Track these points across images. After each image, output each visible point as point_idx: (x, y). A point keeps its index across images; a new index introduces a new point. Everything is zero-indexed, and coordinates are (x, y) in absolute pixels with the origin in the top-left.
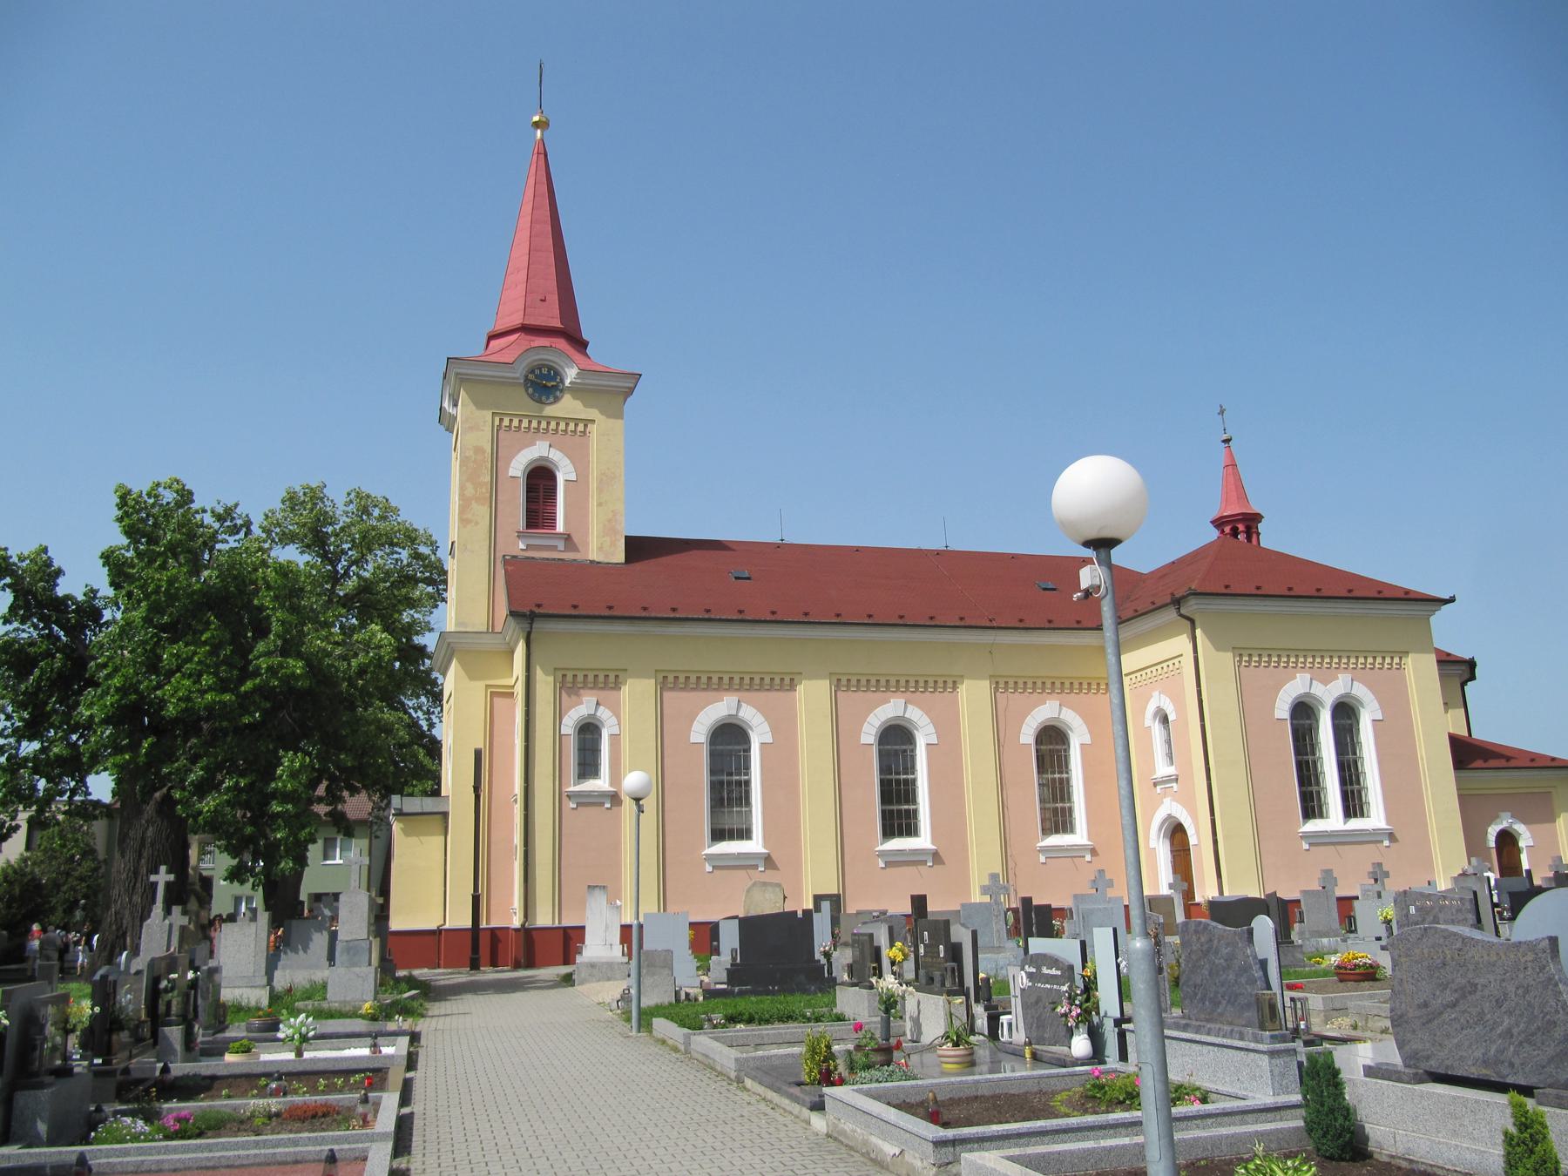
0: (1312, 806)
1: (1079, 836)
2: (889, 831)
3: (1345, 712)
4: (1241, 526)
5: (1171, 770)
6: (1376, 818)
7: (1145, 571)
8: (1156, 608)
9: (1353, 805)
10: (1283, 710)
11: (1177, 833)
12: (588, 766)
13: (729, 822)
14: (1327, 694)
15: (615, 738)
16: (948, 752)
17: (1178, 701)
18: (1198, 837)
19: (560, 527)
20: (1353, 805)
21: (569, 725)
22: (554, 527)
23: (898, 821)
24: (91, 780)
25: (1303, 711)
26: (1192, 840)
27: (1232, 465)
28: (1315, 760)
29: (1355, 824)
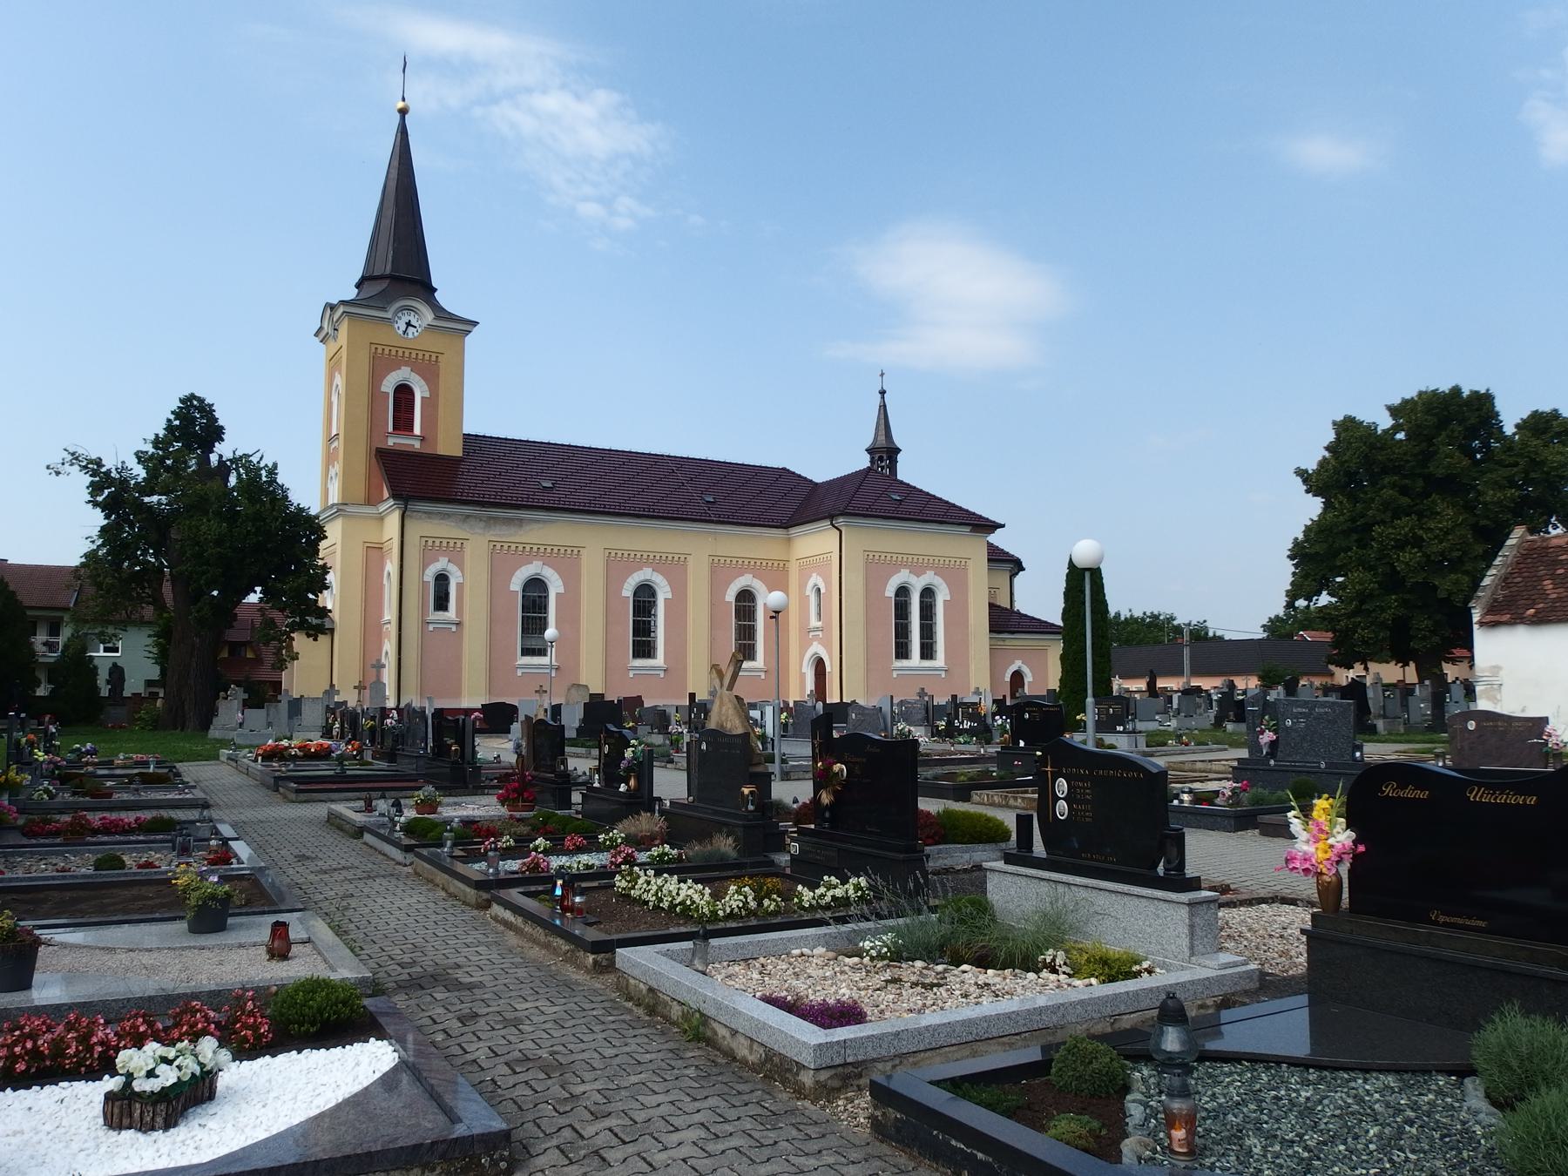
0: (902, 652)
1: (659, 660)
2: (636, 655)
3: (928, 593)
4: (885, 453)
5: (819, 624)
6: (940, 660)
7: (818, 479)
8: (824, 518)
9: (927, 652)
10: (890, 592)
11: (819, 665)
12: (441, 603)
13: (534, 643)
14: (917, 585)
15: (460, 586)
16: (677, 607)
17: (828, 583)
18: (831, 668)
19: (417, 430)
20: (927, 652)
21: (429, 576)
22: (412, 429)
23: (644, 648)
24: (151, 608)
25: (903, 591)
26: (828, 669)
27: (883, 407)
28: (908, 622)
29: (927, 663)
